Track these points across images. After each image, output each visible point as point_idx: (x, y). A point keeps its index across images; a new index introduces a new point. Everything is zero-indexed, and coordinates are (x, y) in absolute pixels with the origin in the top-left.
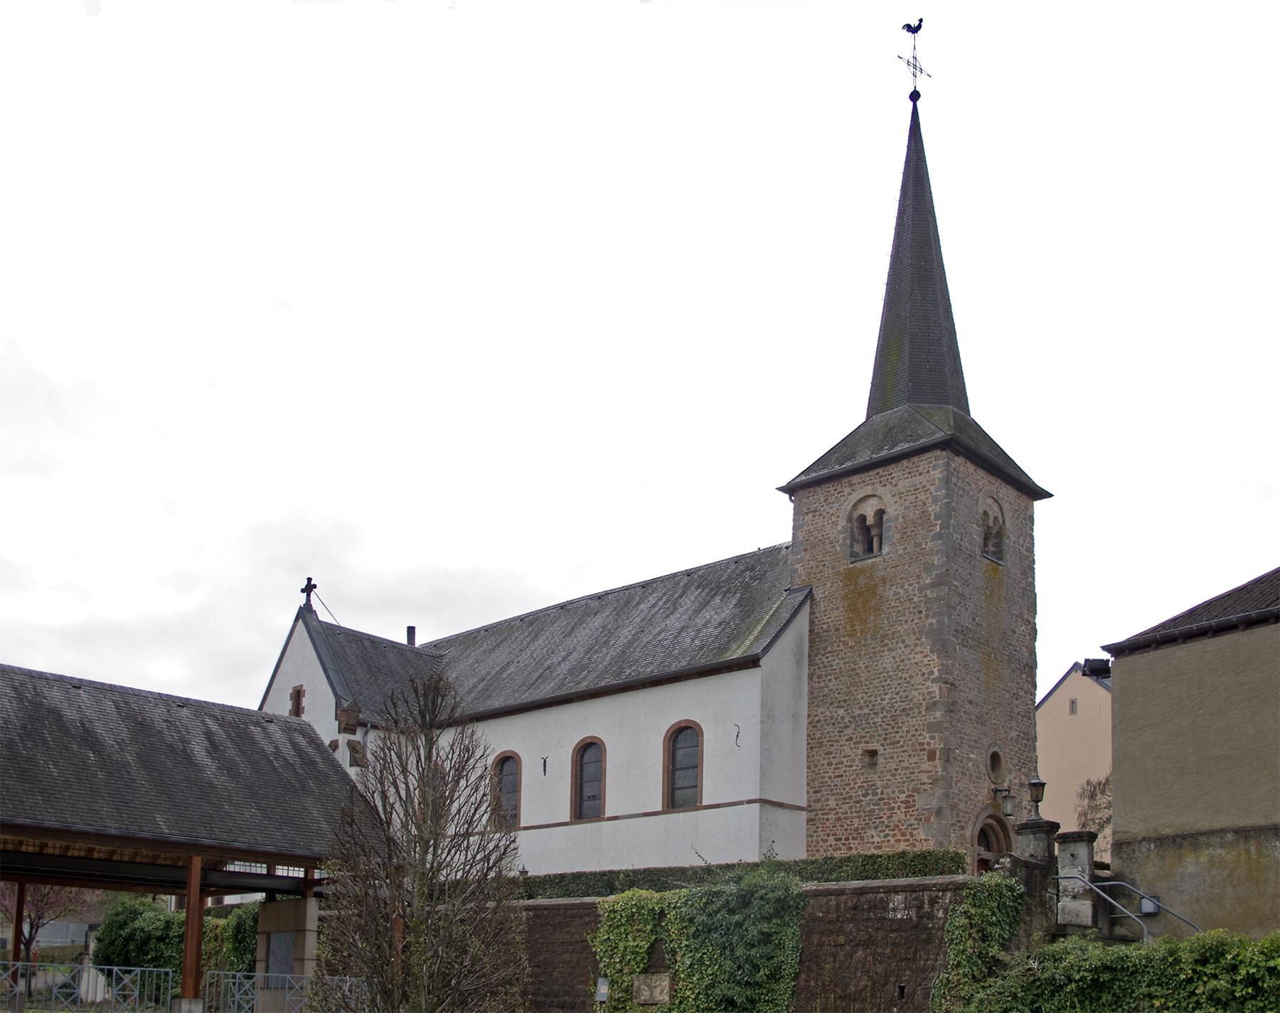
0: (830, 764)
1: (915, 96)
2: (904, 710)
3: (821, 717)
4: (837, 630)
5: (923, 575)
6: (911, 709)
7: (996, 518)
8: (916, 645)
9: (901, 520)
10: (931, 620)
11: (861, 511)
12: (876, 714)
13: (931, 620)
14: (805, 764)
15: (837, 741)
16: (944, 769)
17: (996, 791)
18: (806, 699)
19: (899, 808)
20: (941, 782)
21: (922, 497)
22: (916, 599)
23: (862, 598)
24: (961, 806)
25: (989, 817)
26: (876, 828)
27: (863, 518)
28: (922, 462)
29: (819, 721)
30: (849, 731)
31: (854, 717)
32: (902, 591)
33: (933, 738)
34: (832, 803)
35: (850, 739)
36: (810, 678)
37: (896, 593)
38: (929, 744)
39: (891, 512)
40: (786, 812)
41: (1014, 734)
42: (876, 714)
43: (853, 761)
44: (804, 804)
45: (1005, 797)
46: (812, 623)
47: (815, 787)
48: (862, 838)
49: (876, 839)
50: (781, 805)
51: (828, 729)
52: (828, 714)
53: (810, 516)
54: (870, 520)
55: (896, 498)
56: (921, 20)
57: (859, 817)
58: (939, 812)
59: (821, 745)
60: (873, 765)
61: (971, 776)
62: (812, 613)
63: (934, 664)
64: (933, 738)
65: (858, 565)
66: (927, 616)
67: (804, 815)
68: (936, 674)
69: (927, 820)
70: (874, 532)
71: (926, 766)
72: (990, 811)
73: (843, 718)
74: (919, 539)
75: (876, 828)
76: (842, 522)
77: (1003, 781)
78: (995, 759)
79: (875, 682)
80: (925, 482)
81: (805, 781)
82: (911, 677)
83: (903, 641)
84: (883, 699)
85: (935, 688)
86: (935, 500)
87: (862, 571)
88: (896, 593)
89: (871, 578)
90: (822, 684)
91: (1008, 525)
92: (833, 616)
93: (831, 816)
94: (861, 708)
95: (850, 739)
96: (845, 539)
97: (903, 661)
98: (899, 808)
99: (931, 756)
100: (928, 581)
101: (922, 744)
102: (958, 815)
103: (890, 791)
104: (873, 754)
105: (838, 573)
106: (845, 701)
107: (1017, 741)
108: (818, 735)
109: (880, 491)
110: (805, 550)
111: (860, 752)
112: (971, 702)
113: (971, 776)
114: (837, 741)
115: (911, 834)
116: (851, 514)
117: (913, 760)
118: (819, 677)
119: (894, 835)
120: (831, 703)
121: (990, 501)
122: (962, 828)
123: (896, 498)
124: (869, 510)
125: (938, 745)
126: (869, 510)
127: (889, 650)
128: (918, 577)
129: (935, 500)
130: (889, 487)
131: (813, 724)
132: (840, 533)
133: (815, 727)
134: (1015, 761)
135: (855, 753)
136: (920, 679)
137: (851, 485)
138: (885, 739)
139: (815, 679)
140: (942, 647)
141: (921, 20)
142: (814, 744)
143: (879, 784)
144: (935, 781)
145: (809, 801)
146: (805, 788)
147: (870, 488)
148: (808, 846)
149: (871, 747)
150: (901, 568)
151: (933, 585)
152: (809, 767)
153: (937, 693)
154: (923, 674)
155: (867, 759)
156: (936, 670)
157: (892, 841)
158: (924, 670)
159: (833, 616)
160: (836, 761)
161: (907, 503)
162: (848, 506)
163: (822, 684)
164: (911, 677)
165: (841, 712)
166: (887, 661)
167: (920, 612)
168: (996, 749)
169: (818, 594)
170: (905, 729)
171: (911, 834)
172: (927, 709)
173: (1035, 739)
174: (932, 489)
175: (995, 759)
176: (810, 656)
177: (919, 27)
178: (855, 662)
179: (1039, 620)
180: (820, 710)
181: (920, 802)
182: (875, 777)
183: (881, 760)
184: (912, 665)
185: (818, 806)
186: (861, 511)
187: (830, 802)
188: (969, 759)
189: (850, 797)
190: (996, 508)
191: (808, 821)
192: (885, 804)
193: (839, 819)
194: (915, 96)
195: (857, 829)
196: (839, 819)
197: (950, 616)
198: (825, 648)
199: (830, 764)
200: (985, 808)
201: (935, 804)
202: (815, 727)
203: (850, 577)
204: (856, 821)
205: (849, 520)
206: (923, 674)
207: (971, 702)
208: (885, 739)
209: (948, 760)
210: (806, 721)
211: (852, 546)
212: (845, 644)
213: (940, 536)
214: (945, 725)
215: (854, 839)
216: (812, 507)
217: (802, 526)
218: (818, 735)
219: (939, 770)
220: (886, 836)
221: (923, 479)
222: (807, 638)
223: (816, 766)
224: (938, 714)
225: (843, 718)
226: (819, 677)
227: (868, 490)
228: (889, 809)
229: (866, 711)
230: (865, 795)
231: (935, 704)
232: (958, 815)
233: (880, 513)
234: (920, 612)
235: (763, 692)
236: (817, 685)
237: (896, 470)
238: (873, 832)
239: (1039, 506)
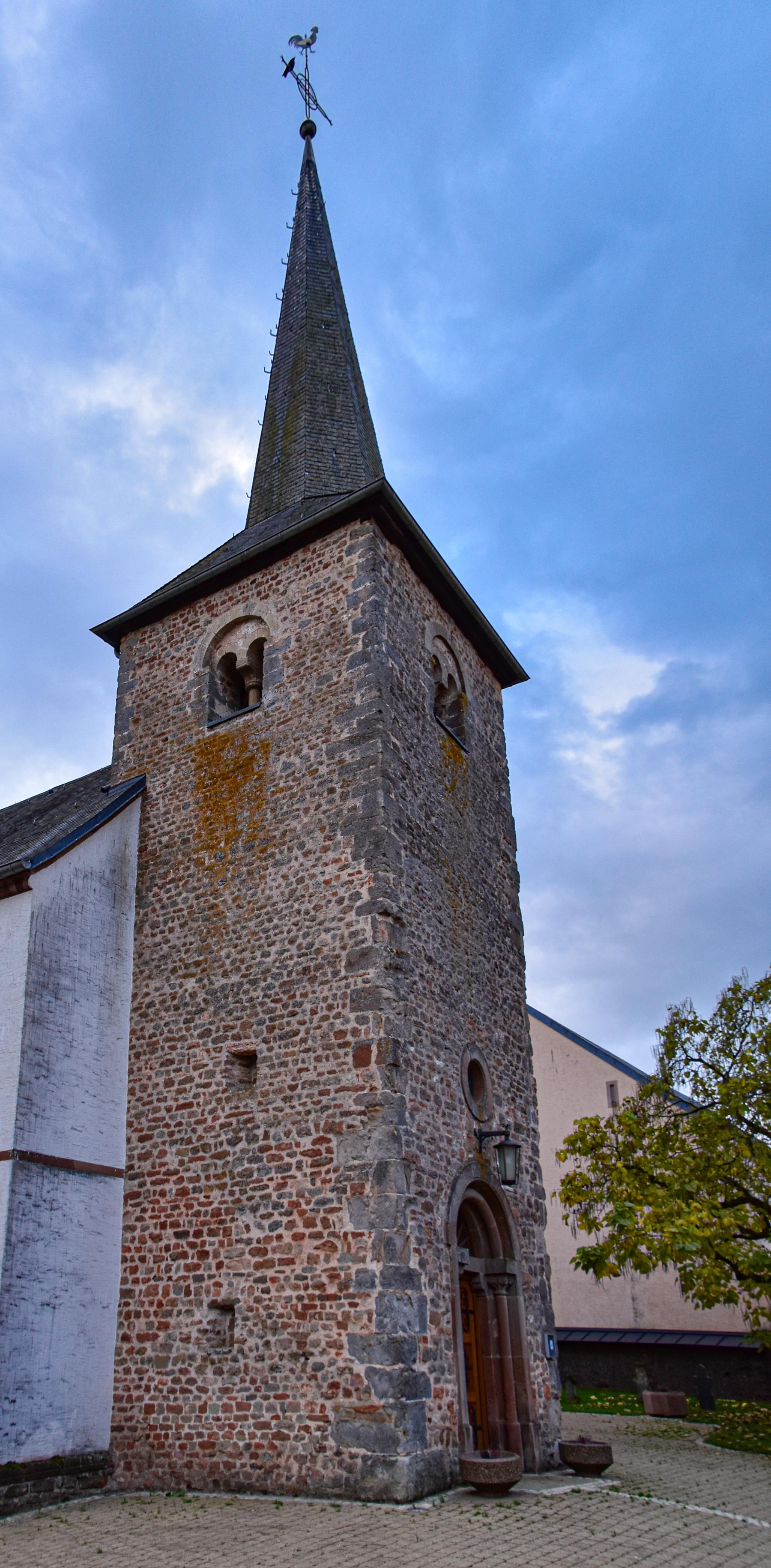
0: (169, 1083)
1: (308, 130)
2: (306, 970)
3: (155, 996)
4: (186, 841)
5: (335, 727)
6: (318, 967)
7: (450, 677)
8: (325, 849)
9: (293, 644)
10: (350, 803)
11: (226, 647)
12: (254, 982)
13: (350, 803)
14: (125, 1085)
15: (183, 1038)
16: (389, 1082)
17: (481, 1136)
18: (130, 966)
19: (299, 1167)
20: (383, 1111)
21: (330, 600)
22: (323, 770)
23: (229, 776)
24: (424, 1161)
25: (472, 1186)
26: (254, 1210)
27: (230, 658)
28: (328, 549)
29: (151, 1005)
30: (203, 1019)
31: (213, 993)
32: (297, 761)
33: (362, 1020)
34: (172, 1161)
35: (206, 1033)
36: (138, 929)
37: (287, 766)
38: (355, 1032)
39: (277, 635)
40: (74, 1180)
41: (500, 1035)
42: (254, 982)
43: (212, 1074)
44: (122, 1164)
45: (500, 1147)
46: (144, 836)
47: (140, 1134)
48: (227, 1232)
49: (256, 1233)
50: (68, 1166)
51: (167, 1016)
52: (167, 990)
53: (145, 667)
54: (242, 660)
55: (286, 612)
56: (315, 30)
57: (222, 1187)
58: (381, 1172)
59: (153, 1047)
60: (249, 1082)
61: (437, 1101)
62: (144, 819)
63: (362, 881)
64: (362, 1020)
65: (221, 730)
66: (344, 797)
67: (119, 1186)
68: (366, 896)
69: (358, 1191)
70: (250, 682)
71: (350, 1077)
72: (474, 1174)
73: (193, 995)
74: (326, 669)
75: (254, 1210)
76: (195, 668)
77: (491, 1117)
78: (475, 1071)
79: (251, 924)
80: (334, 577)
81: (124, 1118)
82: (317, 908)
83: (302, 846)
84: (266, 955)
85: (364, 924)
86: (354, 602)
87: (226, 740)
88: (287, 766)
89: (244, 747)
90: (159, 938)
91: (469, 696)
92: (178, 818)
93: (171, 1187)
94: (225, 974)
95: (206, 1033)
96: (200, 693)
97: (301, 880)
98: (299, 1167)
99: (362, 1058)
100: (345, 735)
101: (341, 1034)
102: (418, 1181)
103: (280, 1130)
104: (248, 1059)
105: (190, 749)
106: (197, 964)
107: (505, 1048)
108: (149, 1030)
109: (257, 607)
110: (136, 721)
111: (223, 1056)
112: (430, 960)
113: (437, 1101)
114: (183, 1038)
115: (325, 1222)
116: (210, 653)
117: (324, 1067)
118: (154, 926)
119: (291, 1225)
120: (174, 971)
121: (439, 643)
122: (428, 1208)
123: (286, 612)
124: (239, 645)
125: (374, 1034)
126: (239, 645)
127: (277, 864)
128: (327, 731)
129: (354, 602)
130: (273, 597)
131: (141, 1011)
132: (192, 684)
133: (144, 1015)
134: (505, 1084)
135: (213, 1059)
136: (334, 910)
137: (210, 609)
138: (271, 1029)
139: (147, 930)
140: (372, 848)
141: (315, 30)
142: (143, 1047)
143: (260, 1117)
144: (371, 1108)
145: (130, 1157)
146: (124, 1132)
147: (241, 606)
148: (126, 1249)
149: (244, 1046)
150: (295, 722)
151: (353, 741)
152: (132, 1092)
153: (369, 933)
154: (340, 901)
155: (237, 1071)
156: (364, 891)
157: (287, 1239)
158: (341, 892)
159: (178, 818)
160: (180, 1076)
161: (305, 617)
162: (205, 641)
163: (159, 938)
164: (317, 908)
165: (191, 984)
166: (273, 885)
167: (332, 791)
168: (476, 1056)
169: (154, 787)
170: (308, 1006)
171: (325, 1221)
172: (350, 965)
173: (530, 1051)
174: (348, 585)
175: (475, 1071)
176: (138, 891)
177: (313, 38)
178: (216, 894)
179: (520, 858)
180: (153, 984)
181: (341, 1154)
182: (253, 1104)
183: (263, 1070)
184: (322, 887)
185: (146, 1166)
186: (226, 647)
187: (167, 1158)
188: (433, 1067)
189: (206, 1147)
190: (451, 662)
191: (128, 1197)
192: (272, 1158)
193: (183, 1192)
194: (308, 130)
195: (216, 1213)
196: (183, 1192)
197: (387, 792)
198: (166, 874)
199: (169, 1083)
200: (466, 1168)
201: (372, 1155)
202: (144, 1015)
203: (208, 751)
204: (216, 1194)
205: (208, 662)
206: (340, 901)
207: (430, 960)
208: (271, 1029)
209: (396, 1065)
210: (128, 1006)
211: (212, 704)
212: (199, 863)
213: (364, 657)
214: (387, 993)
215: (212, 1233)
216: (148, 654)
217: (131, 686)
218: (149, 1030)
219: (378, 1083)
220: (275, 1226)
221: (331, 574)
222: (134, 861)
223: (144, 1088)
224: (372, 973)
225: (193, 995)
226: (154, 926)
227: (239, 611)
228: (280, 1169)
229: (235, 978)
230: (233, 1142)
231: (364, 954)
232: (418, 1181)
233: (257, 647)
234: (332, 791)
235: (34, 936)
236: (149, 941)
237: (285, 570)
238: (247, 1218)
239: (509, 696)
